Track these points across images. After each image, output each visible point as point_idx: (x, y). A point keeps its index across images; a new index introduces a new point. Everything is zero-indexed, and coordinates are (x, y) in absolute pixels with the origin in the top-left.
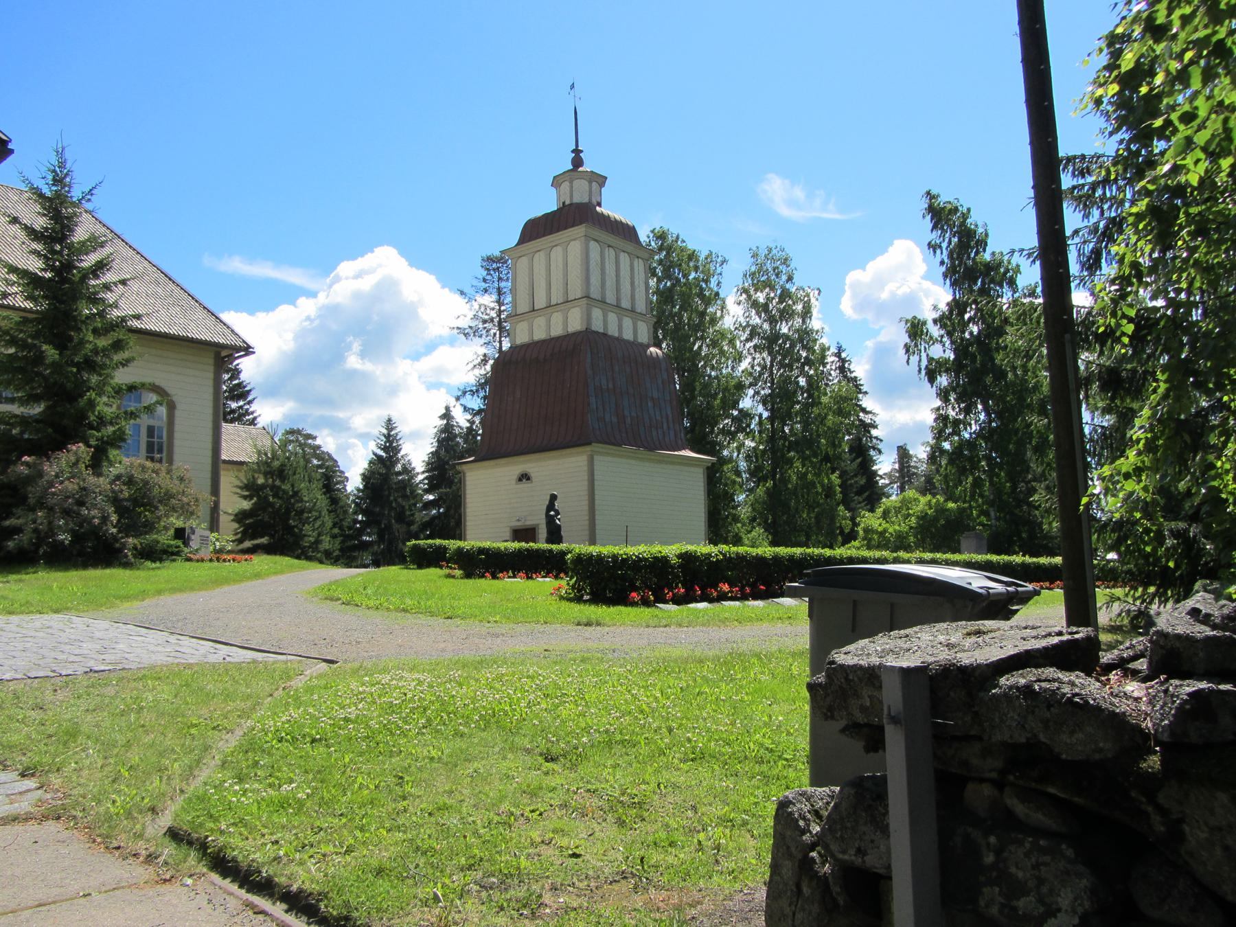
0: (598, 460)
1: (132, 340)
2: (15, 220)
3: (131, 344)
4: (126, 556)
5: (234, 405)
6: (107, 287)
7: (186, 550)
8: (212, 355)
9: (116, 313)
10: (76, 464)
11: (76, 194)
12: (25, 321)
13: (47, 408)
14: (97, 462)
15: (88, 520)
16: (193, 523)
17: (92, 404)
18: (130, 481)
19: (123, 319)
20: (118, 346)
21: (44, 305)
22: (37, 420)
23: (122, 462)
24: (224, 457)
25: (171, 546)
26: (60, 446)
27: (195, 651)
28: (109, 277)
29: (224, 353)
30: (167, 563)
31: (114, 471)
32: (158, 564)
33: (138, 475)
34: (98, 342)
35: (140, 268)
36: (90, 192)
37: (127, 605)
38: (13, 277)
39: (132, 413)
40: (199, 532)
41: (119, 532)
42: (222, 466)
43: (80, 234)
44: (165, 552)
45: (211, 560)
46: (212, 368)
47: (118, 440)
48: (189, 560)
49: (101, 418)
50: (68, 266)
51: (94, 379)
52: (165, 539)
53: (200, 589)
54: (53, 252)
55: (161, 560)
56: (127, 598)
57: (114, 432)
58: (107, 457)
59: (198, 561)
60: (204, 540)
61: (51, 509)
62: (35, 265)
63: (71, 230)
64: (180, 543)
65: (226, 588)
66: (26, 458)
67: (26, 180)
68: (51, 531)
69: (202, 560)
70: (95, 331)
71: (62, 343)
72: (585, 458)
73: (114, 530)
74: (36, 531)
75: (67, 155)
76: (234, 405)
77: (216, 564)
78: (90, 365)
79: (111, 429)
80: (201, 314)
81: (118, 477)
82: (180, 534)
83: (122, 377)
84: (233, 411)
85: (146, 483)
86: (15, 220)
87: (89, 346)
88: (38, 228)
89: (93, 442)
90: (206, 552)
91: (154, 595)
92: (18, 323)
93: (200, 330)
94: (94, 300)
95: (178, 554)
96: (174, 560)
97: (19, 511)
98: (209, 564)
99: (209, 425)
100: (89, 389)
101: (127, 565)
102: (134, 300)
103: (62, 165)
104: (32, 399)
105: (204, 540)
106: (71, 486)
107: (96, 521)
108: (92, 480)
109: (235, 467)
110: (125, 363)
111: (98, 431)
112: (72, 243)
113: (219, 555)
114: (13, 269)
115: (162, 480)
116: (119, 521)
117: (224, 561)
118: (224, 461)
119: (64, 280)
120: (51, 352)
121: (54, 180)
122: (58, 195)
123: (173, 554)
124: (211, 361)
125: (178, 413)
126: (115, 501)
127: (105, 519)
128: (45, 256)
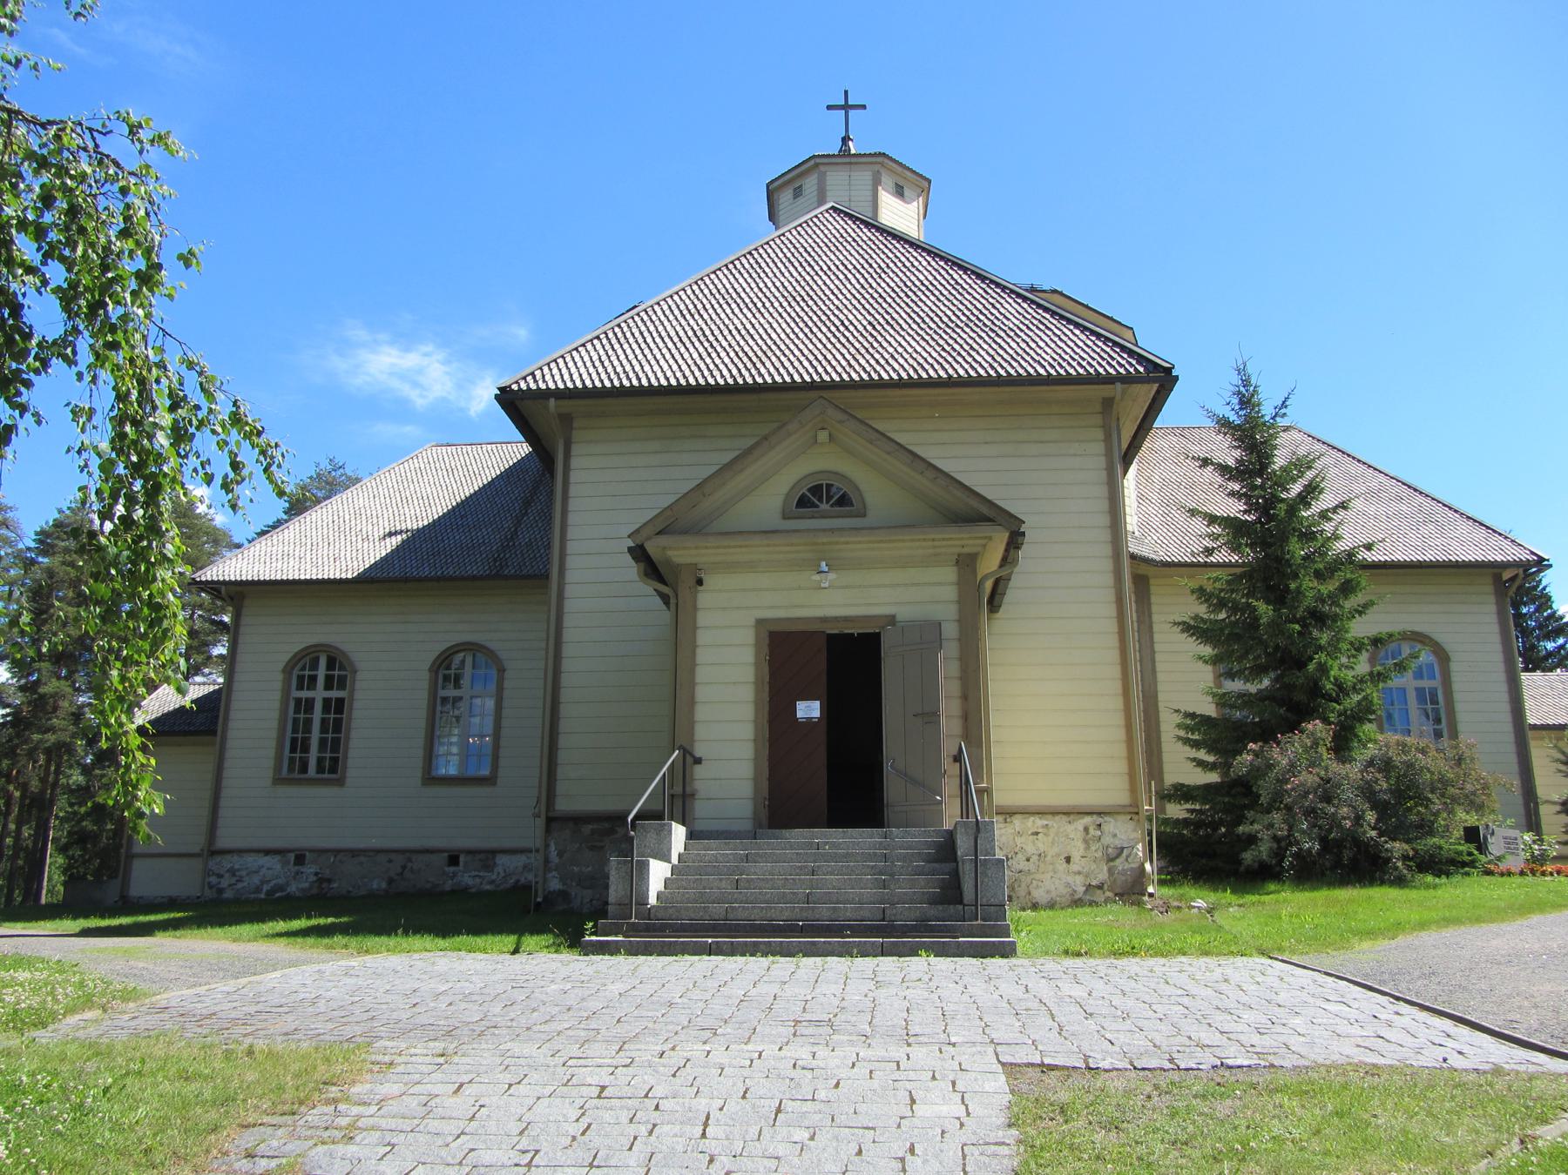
0: (1000, 798)
1: (1364, 578)
2: (1205, 462)
3: (1364, 583)
4: (1396, 868)
5: (1550, 646)
6: (1324, 516)
7: (1482, 858)
8: (1489, 580)
9: (1340, 546)
10: (1316, 744)
11: (1267, 411)
12: (1237, 578)
13: (1277, 680)
14: (1342, 744)
15: (1335, 822)
16: (1488, 819)
17: (1323, 669)
18: (1386, 766)
19: (1350, 554)
20: (1347, 588)
21: (1250, 555)
22: (1262, 697)
23: (1375, 740)
24: (1531, 720)
25: (1460, 853)
26: (1293, 726)
27: (1418, 1041)
28: (1317, 507)
29: (1507, 575)
30: (1457, 878)
31: (1372, 750)
32: (1444, 879)
33: (1398, 759)
34: (1322, 588)
35: (1374, 484)
36: (1284, 405)
37: (1366, 945)
38: (1217, 529)
39: (1379, 674)
40: (1501, 832)
41: (1380, 835)
42: (1530, 734)
43: (1279, 461)
44: (1452, 862)
45: (1522, 873)
46: (1492, 599)
47: (1363, 712)
48: (1489, 873)
49: (1339, 685)
50: (1273, 500)
51: (1324, 638)
52: (1453, 843)
53: (1492, 921)
54: (1253, 487)
55: (1448, 875)
56: (1371, 934)
57: (1359, 703)
58: (1356, 736)
59: (1502, 875)
60: (1510, 843)
61: (1289, 808)
62: (1234, 508)
63: (1270, 456)
64: (1472, 848)
65: (1535, 918)
66: (1251, 746)
67: (1212, 415)
68: (1289, 840)
69: (1509, 874)
70: (1318, 575)
71: (1279, 595)
72: (557, 807)
73: (1374, 833)
74: (1275, 838)
75: (1249, 370)
76: (1550, 646)
77: (1530, 878)
78: (1318, 618)
79: (1356, 698)
80: (1464, 527)
81: (1371, 763)
82: (1472, 834)
83: (1360, 628)
84: (1550, 654)
85: (1410, 765)
86: (1205, 462)
87: (1310, 594)
88: (1231, 463)
89: (1333, 717)
90: (1515, 862)
91: (1413, 929)
92: (1228, 582)
93: (1468, 547)
94: (1308, 536)
95: (1472, 864)
96: (1467, 874)
97: (1250, 814)
98: (1518, 880)
99: (1500, 676)
100: (1320, 648)
101: (1400, 882)
102: (1368, 526)
103: (1246, 383)
104: (1258, 671)
105: (1510, 843)
106: (1308, 778)
107: (1348, 824)
108: (1335, 767)
109: (1553, 734)
110: (1361, 610)
111: (1337, 701)
112: (1274, 472)
113: (1536, 865)
114: (1212, 519)
115: (1434, 763)
116: (1378, 821)
117: (1543, 874)
118: (1534, 727)
119: (1271, 518)
120: (1264, 609)
121: (1241, 402)
122: (1248, 419)
123: (1464, 864)
124: (1490, 588)
125: (1454, 666)
126: (1368, 792)
127: (1358, 819)
128: (1245, 495)
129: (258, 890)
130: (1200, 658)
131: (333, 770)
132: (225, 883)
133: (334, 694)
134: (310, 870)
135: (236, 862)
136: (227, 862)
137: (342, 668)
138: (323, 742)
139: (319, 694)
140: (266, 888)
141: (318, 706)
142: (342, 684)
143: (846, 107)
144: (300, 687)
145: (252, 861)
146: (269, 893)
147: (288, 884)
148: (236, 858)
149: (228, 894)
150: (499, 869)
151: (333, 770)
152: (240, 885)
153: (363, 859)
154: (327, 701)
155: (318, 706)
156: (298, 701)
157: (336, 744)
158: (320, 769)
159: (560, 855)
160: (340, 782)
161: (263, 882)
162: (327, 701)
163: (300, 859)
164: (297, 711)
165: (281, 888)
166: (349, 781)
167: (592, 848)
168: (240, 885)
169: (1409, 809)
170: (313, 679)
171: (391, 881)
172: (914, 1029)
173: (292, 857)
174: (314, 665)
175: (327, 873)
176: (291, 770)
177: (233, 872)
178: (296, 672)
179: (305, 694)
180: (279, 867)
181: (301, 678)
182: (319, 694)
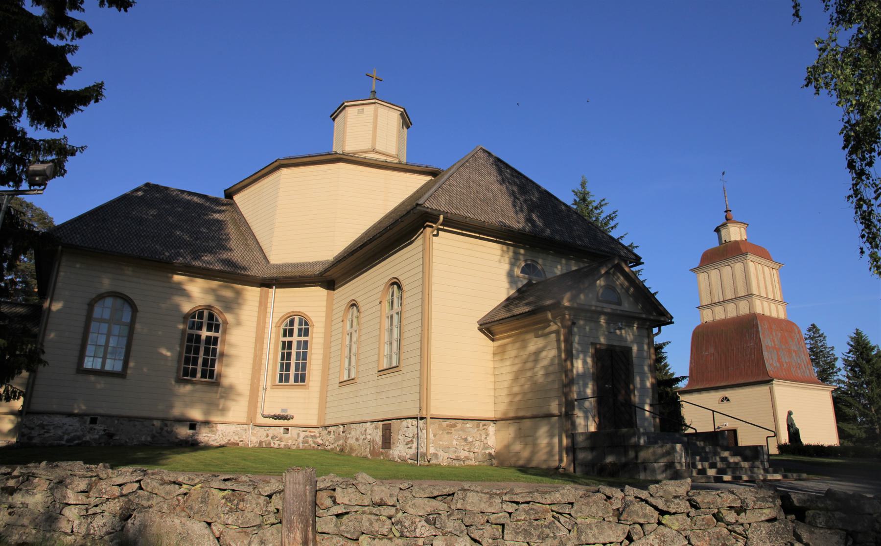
129: (61, 438)
130: (668, 343)
132: (34, 433)
133: (303, 339)
134: (99, 427)
135: (46, 420)
136: (37, 420)
137: (306, 324)
138: (297, 365)
140: (66, 437)
142: (306, 334)
144: (285, 335)
145: (57, 420)
146: (68, 441)
147: (84, 436)
148: (45, 417)
149: (36, 441)
150: (219, 433)
152: (47, 435)
153: (137, 423)
154: (299, 342)
156: (284, 343)
157: (304, 367)
158: (296, 381)
159: (435, 436)
161: (64, 433)
162: (299, 342)
163: (94, 421)
164: (283, 348)
165: (79, 438)
167: (448, 433)
168: (47, 435)
171: (153, 437)
172: (69, 531)
173: (88, 419)
174: (292, 323)
175: (112, 430)
176: (281, 381)
177: (42, 426)
178: (283, 327)
179: (287, 339)
180: (78, 425)
181: (285, 331)
182: (295, 339)
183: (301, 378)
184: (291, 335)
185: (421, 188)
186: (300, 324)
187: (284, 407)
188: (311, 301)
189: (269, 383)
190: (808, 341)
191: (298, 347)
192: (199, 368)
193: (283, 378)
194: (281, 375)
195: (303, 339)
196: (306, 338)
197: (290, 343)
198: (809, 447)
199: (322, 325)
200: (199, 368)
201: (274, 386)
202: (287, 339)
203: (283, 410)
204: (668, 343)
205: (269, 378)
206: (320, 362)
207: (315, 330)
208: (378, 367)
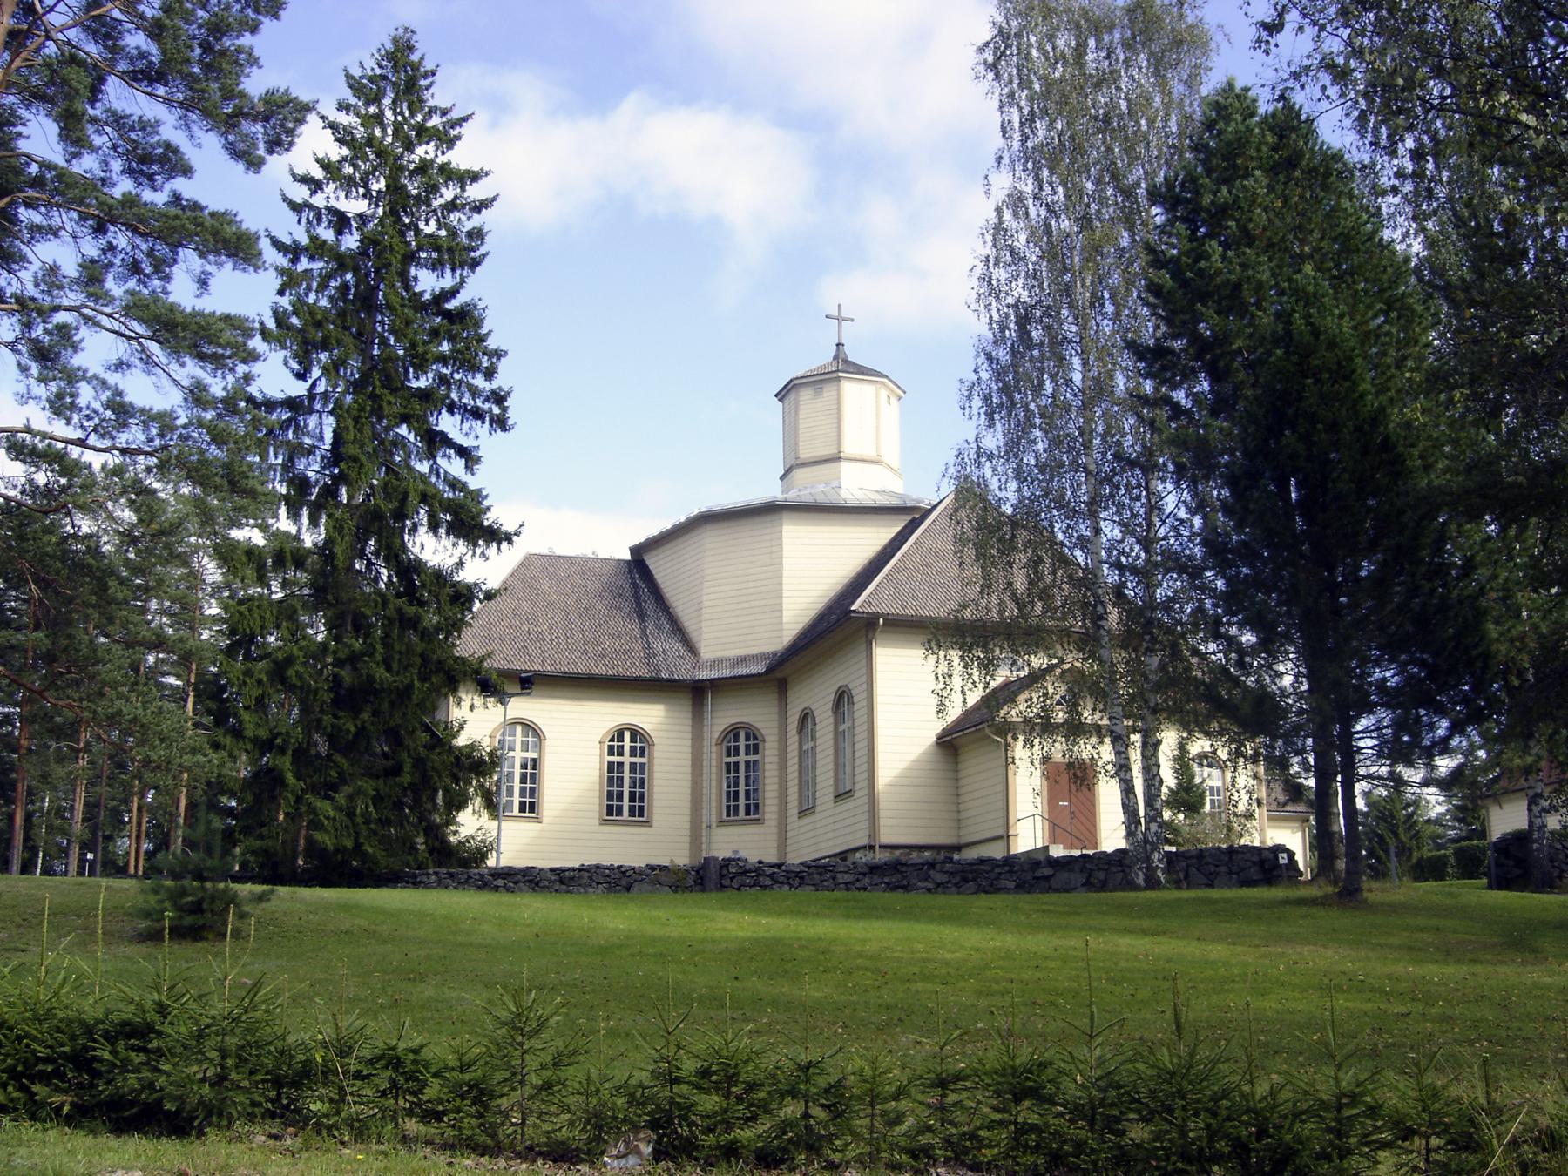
9: (461, 741)
130: (285, 199)
131: (532, 810)
133: (752, 758)
137: (756, 738)
139: (742, 758)
141: (627, 768)
142: (756, 752)
143: (840, 319)
144: (729, 755)
151: (532, 810)
155: (627, 768)
156: (728, 764)
160: (647, 823)
162: (633, 765)
164: (728, 772)
166: (655, 824)
169: (1542, 64)
170: (737, 749)
174: (736, 738)
178: (725, 744)
179: (732, 759)
181: (728, 749)
182: (742, 758)
183: (753, 809)
184: (737, 752)
185: (885, 548)
186: (747, 739)
187: (735, 847)
188: (757, 713)
189: (714, 818)
190: (166, 1067)
191: (747, 770)
192: (626, 803)
193: (732, 810)
194: (728, 807)
195: (752, 758)
196: (612, 759)
197: (736, 764)
198: (1518, 795)
199: (775, 738)
200: (626, 803)
201: (721, 823)
202: (732, 759)
203: (736, 852)
204: (285, 199)
205: (714, 811)
206: (776, 787)
207: (767, 745)
208: (836, 788)
